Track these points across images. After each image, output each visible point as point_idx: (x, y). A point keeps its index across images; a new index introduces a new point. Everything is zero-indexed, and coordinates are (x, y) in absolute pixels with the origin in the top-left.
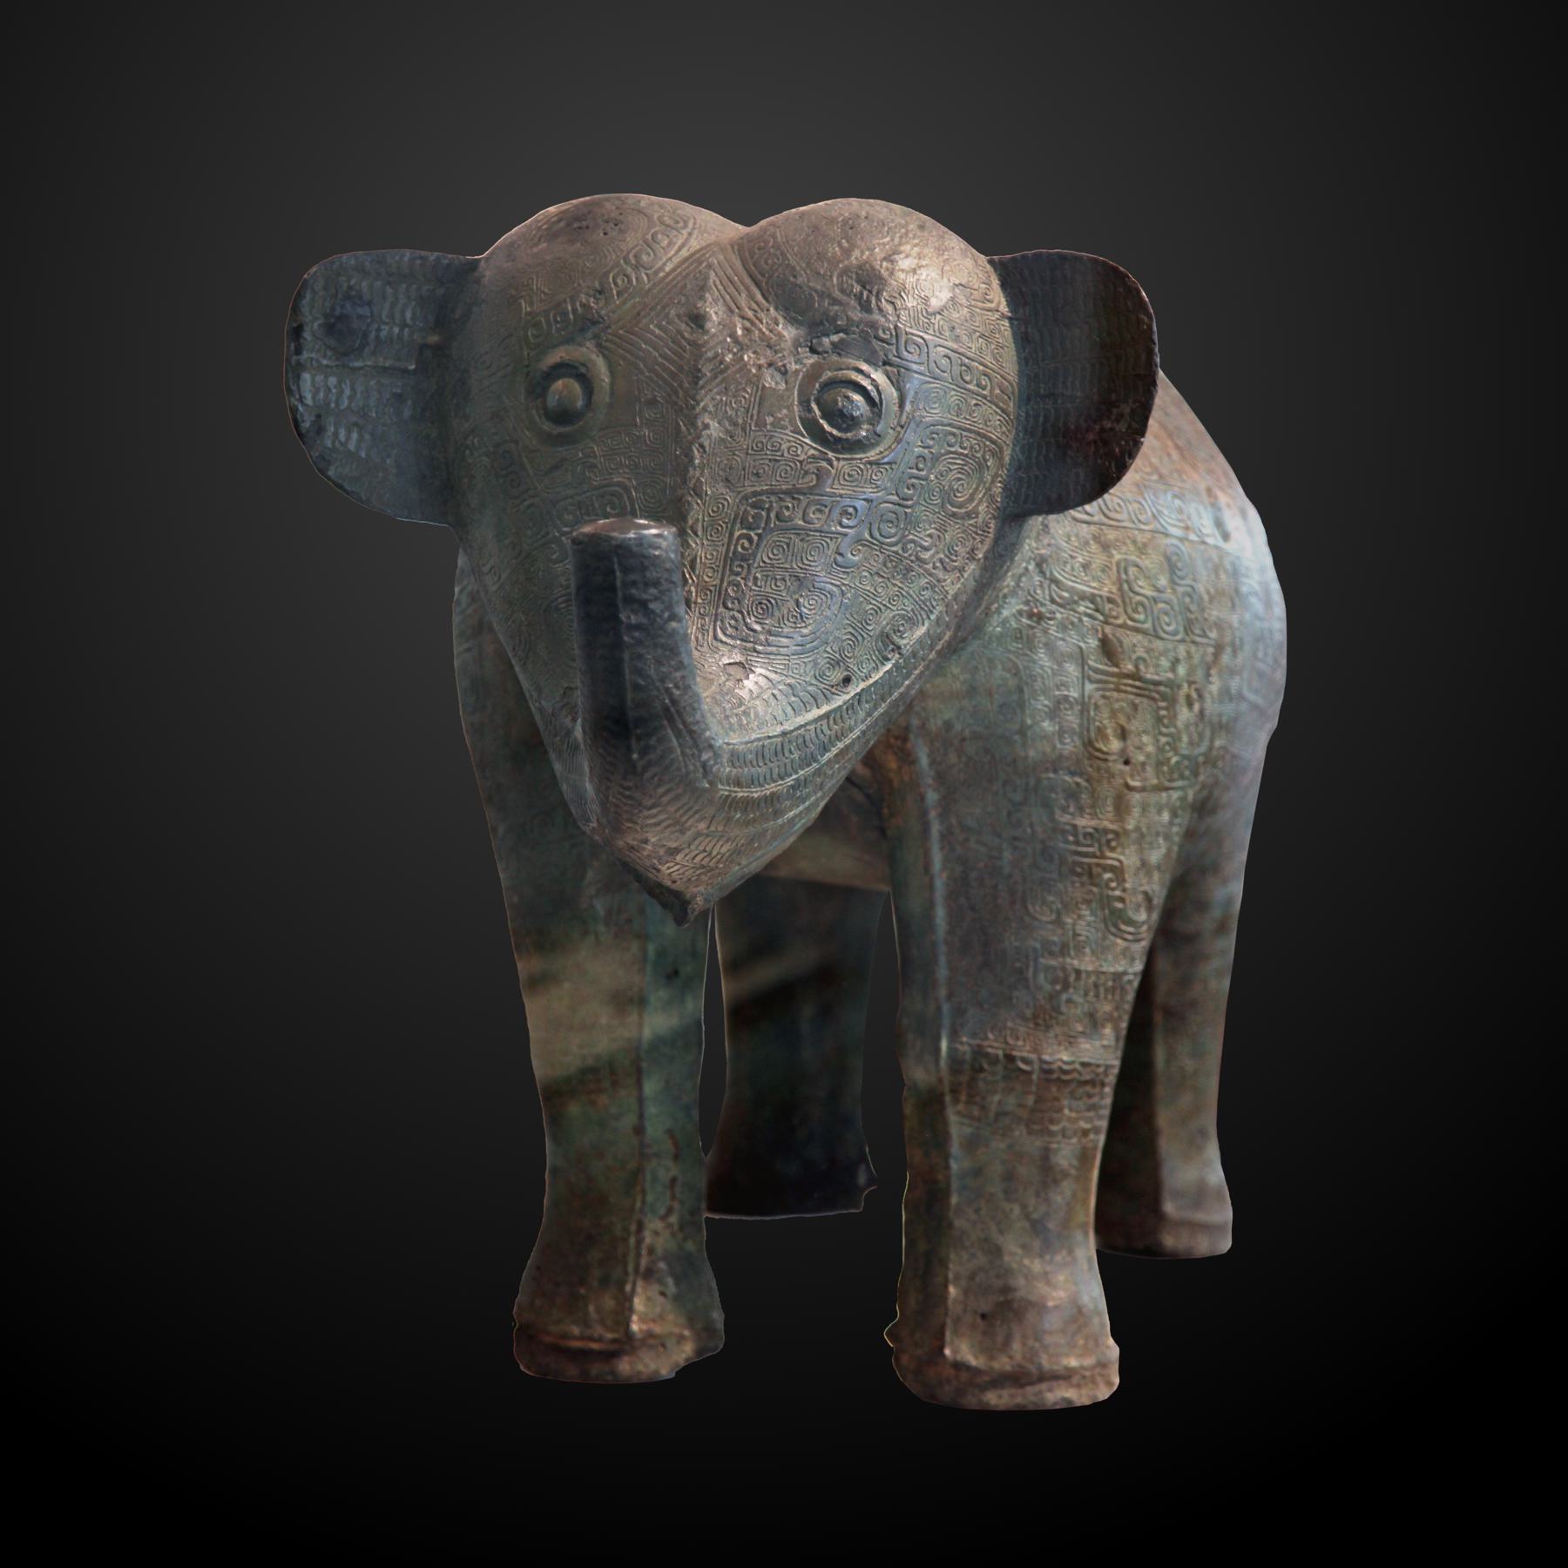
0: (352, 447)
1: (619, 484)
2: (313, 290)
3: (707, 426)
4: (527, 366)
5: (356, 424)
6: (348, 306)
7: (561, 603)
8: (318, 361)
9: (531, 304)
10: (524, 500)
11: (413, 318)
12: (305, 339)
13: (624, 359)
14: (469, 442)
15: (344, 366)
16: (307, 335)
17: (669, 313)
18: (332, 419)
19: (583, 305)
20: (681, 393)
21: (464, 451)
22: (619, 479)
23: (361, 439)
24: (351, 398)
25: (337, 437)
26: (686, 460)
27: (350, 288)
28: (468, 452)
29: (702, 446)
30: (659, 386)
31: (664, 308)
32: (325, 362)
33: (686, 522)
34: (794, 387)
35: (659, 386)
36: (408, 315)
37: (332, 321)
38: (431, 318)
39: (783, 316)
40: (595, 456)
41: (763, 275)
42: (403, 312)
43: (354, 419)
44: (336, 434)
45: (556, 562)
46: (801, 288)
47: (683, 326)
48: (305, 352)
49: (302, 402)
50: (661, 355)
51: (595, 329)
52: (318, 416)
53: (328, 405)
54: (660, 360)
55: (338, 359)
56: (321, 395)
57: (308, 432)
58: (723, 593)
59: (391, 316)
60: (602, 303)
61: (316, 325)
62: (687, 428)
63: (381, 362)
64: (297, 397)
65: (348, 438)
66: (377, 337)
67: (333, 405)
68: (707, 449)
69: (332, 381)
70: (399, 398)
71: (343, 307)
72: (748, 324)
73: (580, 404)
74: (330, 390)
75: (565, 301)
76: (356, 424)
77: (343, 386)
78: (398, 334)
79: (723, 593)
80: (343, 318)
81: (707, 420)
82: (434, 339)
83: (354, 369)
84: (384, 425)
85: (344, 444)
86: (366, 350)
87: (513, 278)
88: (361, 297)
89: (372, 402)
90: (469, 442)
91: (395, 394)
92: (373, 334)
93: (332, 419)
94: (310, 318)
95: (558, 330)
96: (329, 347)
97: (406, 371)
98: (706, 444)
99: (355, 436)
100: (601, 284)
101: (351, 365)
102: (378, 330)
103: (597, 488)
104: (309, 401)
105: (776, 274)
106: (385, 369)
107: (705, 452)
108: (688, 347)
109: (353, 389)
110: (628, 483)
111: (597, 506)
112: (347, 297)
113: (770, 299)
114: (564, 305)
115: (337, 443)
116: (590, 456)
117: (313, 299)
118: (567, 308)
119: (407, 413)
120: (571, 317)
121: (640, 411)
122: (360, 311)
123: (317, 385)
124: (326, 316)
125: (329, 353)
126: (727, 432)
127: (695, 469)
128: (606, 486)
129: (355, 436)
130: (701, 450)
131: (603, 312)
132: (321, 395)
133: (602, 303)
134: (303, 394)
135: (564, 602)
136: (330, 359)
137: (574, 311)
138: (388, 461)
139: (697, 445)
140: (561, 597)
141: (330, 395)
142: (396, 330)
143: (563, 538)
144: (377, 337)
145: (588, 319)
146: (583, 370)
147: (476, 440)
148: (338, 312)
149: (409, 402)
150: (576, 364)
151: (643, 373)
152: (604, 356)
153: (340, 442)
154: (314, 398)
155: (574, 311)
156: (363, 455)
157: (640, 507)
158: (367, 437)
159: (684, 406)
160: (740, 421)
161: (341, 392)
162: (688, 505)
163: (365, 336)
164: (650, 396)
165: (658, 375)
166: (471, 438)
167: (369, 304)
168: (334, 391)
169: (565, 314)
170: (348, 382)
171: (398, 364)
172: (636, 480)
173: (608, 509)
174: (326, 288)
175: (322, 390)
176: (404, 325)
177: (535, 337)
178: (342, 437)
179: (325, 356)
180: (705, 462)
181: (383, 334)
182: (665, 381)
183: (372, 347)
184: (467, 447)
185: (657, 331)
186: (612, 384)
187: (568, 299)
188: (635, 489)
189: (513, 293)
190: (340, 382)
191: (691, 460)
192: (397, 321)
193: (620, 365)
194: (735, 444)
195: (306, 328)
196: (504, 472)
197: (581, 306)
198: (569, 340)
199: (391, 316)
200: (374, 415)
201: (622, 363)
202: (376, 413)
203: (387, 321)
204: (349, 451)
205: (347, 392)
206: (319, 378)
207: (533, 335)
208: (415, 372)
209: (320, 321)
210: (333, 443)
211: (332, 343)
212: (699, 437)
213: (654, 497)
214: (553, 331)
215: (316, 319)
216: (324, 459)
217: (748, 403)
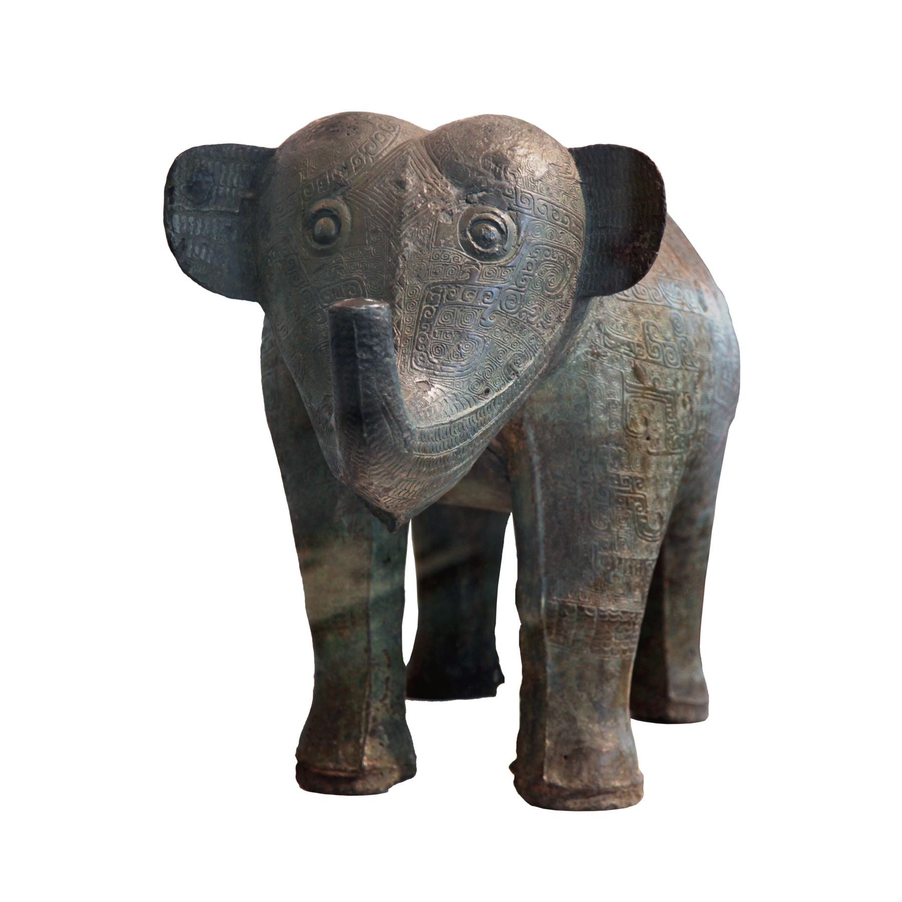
0: (202, 257)
1: (356, 279)
2: (180, 167)
3: (406, 245)
4: (303, 211)
5: (205, 244)
6: (200, 176)
7: (323, 347)
8: (183, 207)
9: (306, 175)
10: (302, 288)
11: (238, 183)
12: (176, 195)
13: (359, 206)
14: (270, 254)
15: (198, 211)
16: (177, 193)
17: (385, 180)
18: (191, 241)
19: (335, 176)
20: (392, 226)
21: (267, 260)
22: (356, 276)
23: (208, 253)
24: (202, 229)
25: (194, 252)
26: (395, 264)
27: (201, 166)
28: (269, 260)
29: (404, 257)
30: (379, 222)
31: (382, 177)
32: (187, 208)
33: (395, 300)
34: (457, 223)
35: (379, 222)
36: (235, 181)
37: (191, 184)
38: (248, 183)
39: (450, 182)
41: (439, 158)
42: (232, 180)
44: (193, 250)
45: (320, 323)
47: (393, 188)
48: (175, 203)
49: (174, 231)
52: (183, 239)
53: (189, 233)
54: (380, 207)
56: (185, 227)
57: (177, 248)
58: (416, 341)
60: (346, 174)
61: (182, 187)
62: (395, 246)
63: (219, 208)
64: (171, 228)
65: (200, 252)
66: (217, 194)
67: (191, 233)
68: (407, 258)
69: (191, 219)
70: (230, 229)
71: (197, 176)
72: (430, 187)
73: (333, 232)
74: (190, 224)
75: (325, 173)
76: (205, 244)
77: (198, 222)
78: (229, 192)
79: (416, 341)
80: (197, 183)
81: (407, 242)
82: (249, 195)
83: (204, 213)
85: (198, 256)
86: (211, 201)
87: (295, 160)
88: (207, 171)
89: (214, 231)
91: (227, 227)
92: (215, 192)
93: (191, 241)
94: (178, 183)
96: (189, 200)
97: (233, 213)
98: (406, 255)
99: (204, 251)
100: (346, 163)
101: (202, 210)
102: (218, 190)
103: (343, 281)
104: (178, 231)
105: (447, 158)
106: (221, 212)
107: (405, 260)
108: (396, 200)
109: (203, 224)
110: (361, 278)
111: (343, 291)
113: (443, 172)
114: (324, 176)
115: (194, 255)
116: (339, 262)
117: (180, 172)
118: (326, 177)
119: (234, 238)
120: (329, 182)
121: (368, 236)
122: (207, 179)
123: (182, 222)
124: (187, 182)
125: (189, 203)
126: (418, 248)
127: (400, 270)
128: (348, 279)
129: (204, 251)
131: (347, 180)
132: (185, 227)
133: (346, 174)
135: (324, 346)
136: (190, 206)
137: (330, 179)
138: (223, 265)
140: (323, 343)
141: (190, 227)
142: (228, 190)
143: (324, 310)
144: (217, 194)
145: (338, 184)
146: (335, 213)
147: (274, 253)
148: (194, 179)
149: (236, 231)
150: (332, 210)
151: (370, 215)
152: (348, 205)
153: (196, 254)
154: (180, 229)
156: (209, 262)
157: (368, 292)
158: (211, 251)
159: (393, 233)
160: (426, 242)
161: (196, 226)
162: (396, 291)
163: (210, 193)
164: (374, 228)
165: (378, 216)
166: (271, 252)
167: (212, 175)
168: (192, 225)
169: (325, 181)
170: (200, 220)
171: (229, 209)
172: (366, 276)
173: (350, 293)
174: (187, 166)
176: (232, 187)
177: (308, 194)
178: (197, 251)
179: (187, 205)
181: (220, 192)
182: (382, 219)
183: (214, 200)
184: (269, 257)
185: (378, 190)
186: (352, 221)
187: (327, 172)
189: (295, 168)
190: (195, 220)
191: (398, 264)
192: (228, 185)
193: (357, 210)
195: (176, 189)
196: (290, 272)
197: (334, 176)
198: (328, 196)
199: (225, 182)
200: (215, 239)
201: (358, 209)
202: (217, 237)
203: (223, 184)
204: (201, 259)
205: (200, 225)
206: (184, 217)
207: (307, 193)
208: (238, 214)
209: (184, 185)
210: (192, 255)
211: (191, 197)
212: (402, 251)
213: (376, 286)
214: (318, 191)
215: (182, 183)
216: (186, 264)
217: (430, 232)
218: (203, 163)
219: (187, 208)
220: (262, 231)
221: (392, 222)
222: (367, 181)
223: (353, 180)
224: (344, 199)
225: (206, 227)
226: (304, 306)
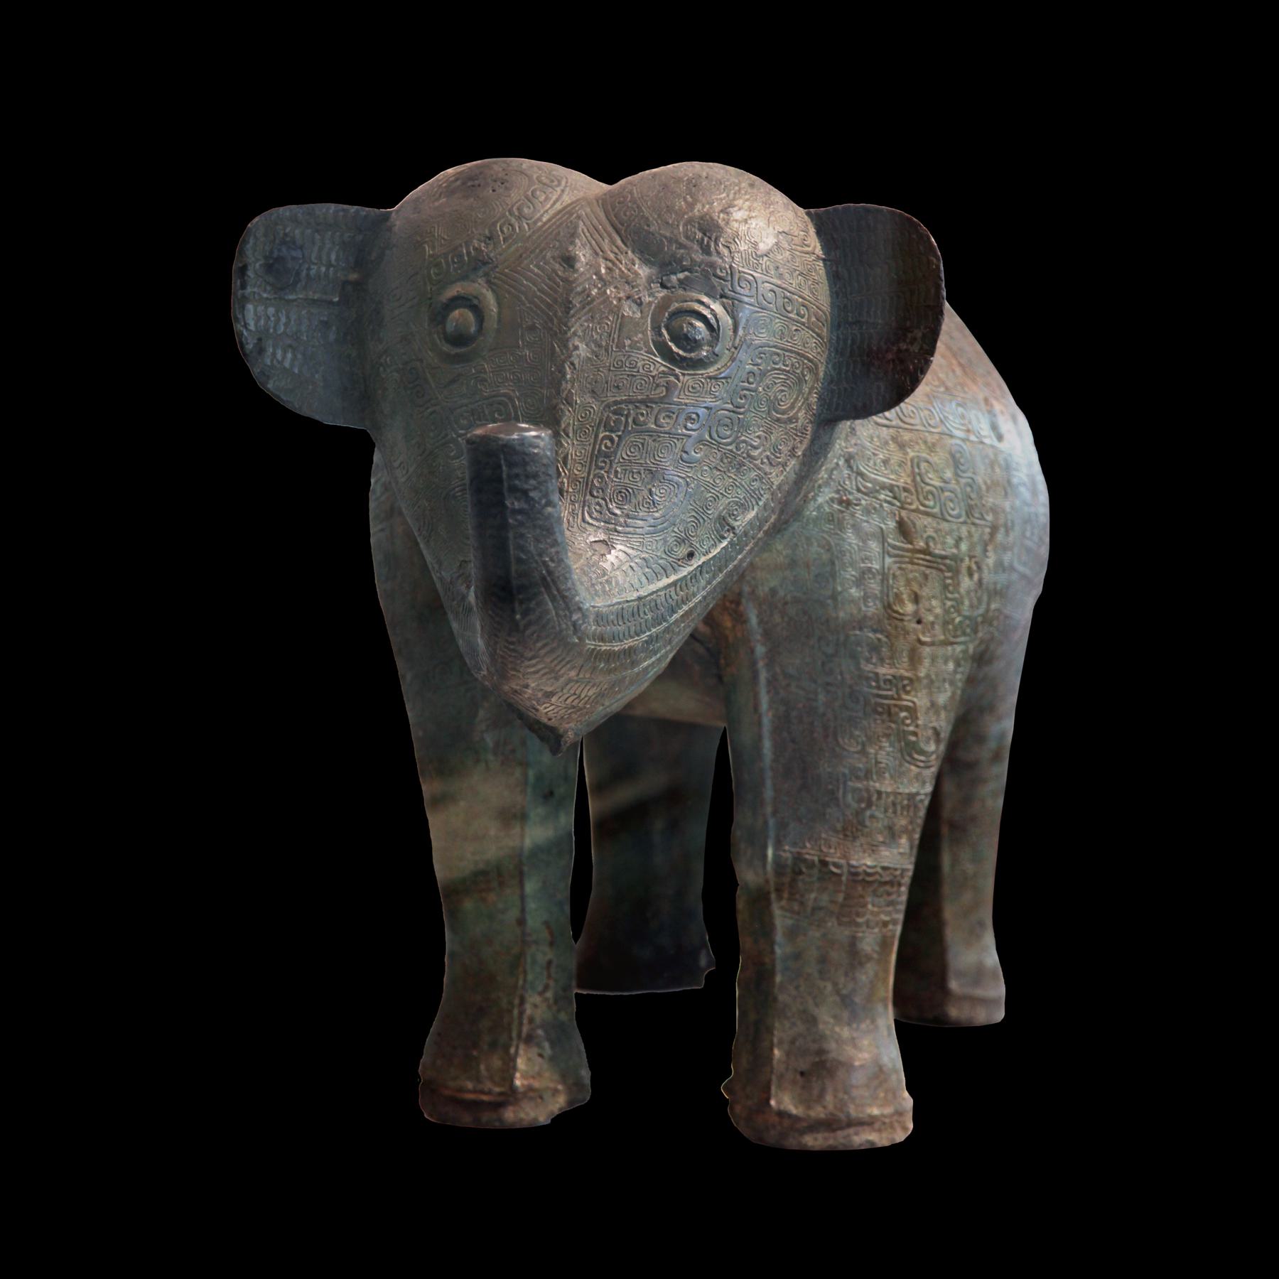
0: (287, 364)
1: (505, 395)
4: (430, 299)
5: (290, 346)
6: (284, 249)
7: (457, 492)
8: (259, 294)
9: (433, 248)
10: (428, 408)
11: (337, 260)
12: (249, 277)
13: (509, 293)
14: (382, 361)
15: (281, 299)
16: (250, 273)
17: (545, 255)
18: (270, 342)
19: (476, 249)
20: (555, 321)
21: (379, 368)
22: (505, 391)
23: (294, 358)
24: (286, 325)
25: (275, 357)
28: (381, 369)
29: (572, 364)
30: (538, 315)
31: (541, 251)
32: (265, 295)
33: (560, 426)
34: (648, 316)
36: (333, 257)
37: (271, 262)
38: (351, 259)
39: (638, 258)
40: (485, 372)
41: (622, 225)
42: (329, 255)
43: (289, 342)
44: (274, 354)
45: (453, 458)
46: (653, 235)
47: (557, 266)
48: (248, 287)
50: (539, 290)
51: (485, 269)
52: (260, 340)
53: (268, 330)
54: (538, 293)
55: (275, 293)
56: (262, 322)
58: (590, 483)
59: (319, 258)
60: (491, 247)
61: (257, 265)
62: (560, 349)
63: (311, 295)
64: (243, 324)
65: (284, 357)
66: (308, 275)
67: (271, 331)
68: (577, 366)
69: (271, 310)
70: (326, 325)
71: (279, 250)
73: (473, 329)
75: (461, 246)
76: (290, 346)
77: (280, 315)
78: (325, 273)
79: (590, 483)
80: (280, 259)
81: (577, 343)
82: (354, 276)
83: (289, 301)
84: (313, 347)
85: (281, 363)
86: (299, 285)
87: (418, 227)
88: (294, 243)
89: (303, 328)
90: (382, 361)
91: (322, 322)
92: (304, 273)
93: (270, 342)
94: (253, 259)
95: (455, 269)
96: (268, 283)
97: (331, 303)
99: (289, 355)
100: (490, 232)
101: (286, 297)
102: (309, 269)
103: (487, 398)
104: (252, 327)
105: (633, 224)
106: (314, 301)
107: (575, 368)
108: (561, 283)
109: (288, 317)
110: (512, 394)
111: (487, 412)
112: (283, 243)
113: (628, 244)
114: (460, 249)
115: (275, 362)
116: (481, 372)
117: (255, 244)
118: (462, 252)
119: (332, 337)
121: (522, 335)
122: (294, 253)
123: (259, 314)
124: (266, 258)
125: (268, 288)
126: (593, 352)
127: (567, 382)
128: (494, 396)
129: (289, 355)
130: (572, 367)
131: (492, 255)
132: (262, 322)
133: (491, 247)
134: (247, 322)
135: (460, 491)
136: (269, 292)
137: (469, 253)
138: (317, 376)
139: (569, 363)
140: (458, 487)
141: (269, 322)
142: (323, 269)
143: (459, 439)
144: (308, 275)
145: (480, 261)
146: (476, 302)
147: (388, 359)
148: (276, 254)
149: (334, 328)
150: (470, 297)
151: (524, 304)
152: (493, 291)
153: (278, 360)
154: (256, 325)
155: (469, 253)
156: (296, 371)
157: (522, 414)
158: (299, 356)
159: (558, 331)
160: (604, 344)
161: (278, 320)
162: (562, 412)
163: (298, 274)
165: (537, 306)
166: (384, 357)
167: (301, 248)
168: (272, 319)
169: (461, 256)
170: (284, 312)
171: (324, 297)
172: (519, 391)
173: (496, 416)
174: (266, 235)
175: (263, 318)
176: (329, 265)
177: (437, 274)
178: (279, 356)
179: (265, 291)
180: (575, 376)
181: (313, 272)
182: (542, 311)
183: (304, 283)
184: (381, 365)
185: (536, 270)
186: (499, 313)
187: (463, 244)
188: (518, 399)
189: (419, 239)
190: (277, 312)
191: (564, 375)
192: (324, 262)
193: (506, 298)
194: (599, 362)
195: (249, 268)
196: (411, 385)
197: (474, 249)
198: (464, 277)
199: (319, 258)
200: (305, 338)
201: (507, 296)
202: (307, 337)
203: (316, 261)
204: (285, 368)
205: (283, 320)
206: (261, 308)
208: (338, 303)
209: (261, 262)
210: (272, 361)
211: (271, 279)
212: (570, 356)
213: (533, 405)
214: (451, 270)
215: (258, 260)
216: (264, 374)
217: (610, 329)
218: (287, 230)
219: (265, 295)
220: (371, 327)
221: (555, 314)
222: (521, 256)
223: (500, 255)
224: (488, 282)
225: (292, 322)
226: (432, 434)
